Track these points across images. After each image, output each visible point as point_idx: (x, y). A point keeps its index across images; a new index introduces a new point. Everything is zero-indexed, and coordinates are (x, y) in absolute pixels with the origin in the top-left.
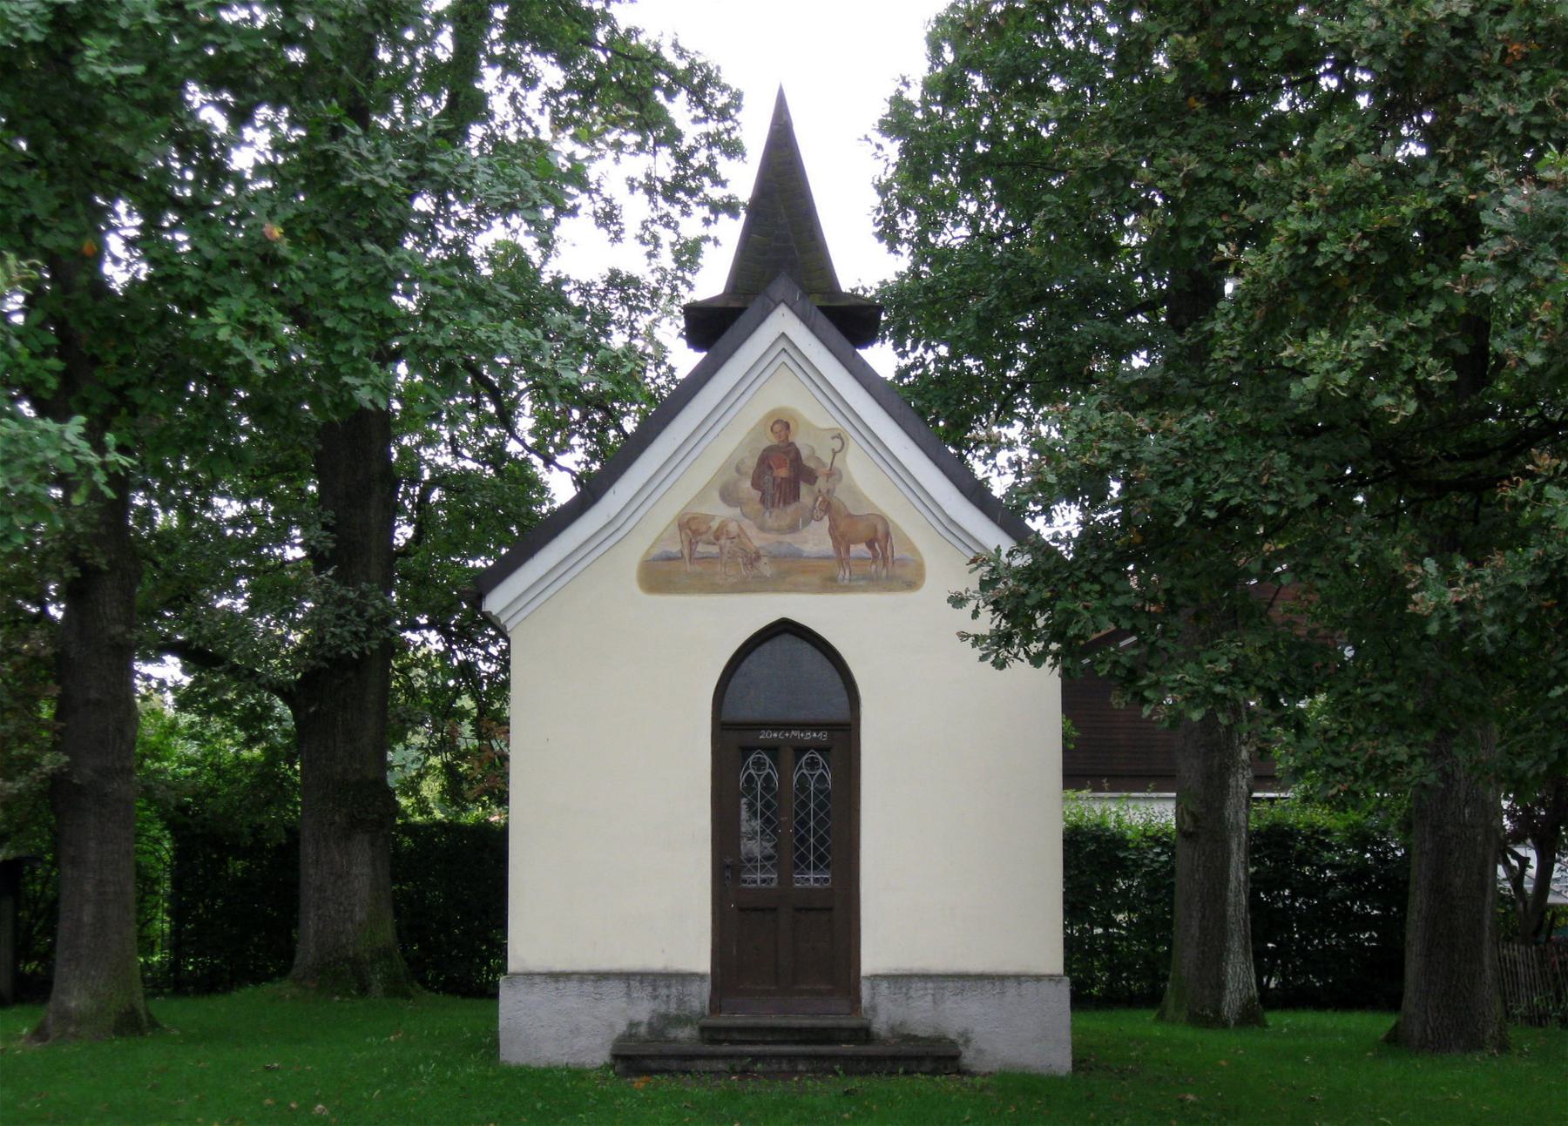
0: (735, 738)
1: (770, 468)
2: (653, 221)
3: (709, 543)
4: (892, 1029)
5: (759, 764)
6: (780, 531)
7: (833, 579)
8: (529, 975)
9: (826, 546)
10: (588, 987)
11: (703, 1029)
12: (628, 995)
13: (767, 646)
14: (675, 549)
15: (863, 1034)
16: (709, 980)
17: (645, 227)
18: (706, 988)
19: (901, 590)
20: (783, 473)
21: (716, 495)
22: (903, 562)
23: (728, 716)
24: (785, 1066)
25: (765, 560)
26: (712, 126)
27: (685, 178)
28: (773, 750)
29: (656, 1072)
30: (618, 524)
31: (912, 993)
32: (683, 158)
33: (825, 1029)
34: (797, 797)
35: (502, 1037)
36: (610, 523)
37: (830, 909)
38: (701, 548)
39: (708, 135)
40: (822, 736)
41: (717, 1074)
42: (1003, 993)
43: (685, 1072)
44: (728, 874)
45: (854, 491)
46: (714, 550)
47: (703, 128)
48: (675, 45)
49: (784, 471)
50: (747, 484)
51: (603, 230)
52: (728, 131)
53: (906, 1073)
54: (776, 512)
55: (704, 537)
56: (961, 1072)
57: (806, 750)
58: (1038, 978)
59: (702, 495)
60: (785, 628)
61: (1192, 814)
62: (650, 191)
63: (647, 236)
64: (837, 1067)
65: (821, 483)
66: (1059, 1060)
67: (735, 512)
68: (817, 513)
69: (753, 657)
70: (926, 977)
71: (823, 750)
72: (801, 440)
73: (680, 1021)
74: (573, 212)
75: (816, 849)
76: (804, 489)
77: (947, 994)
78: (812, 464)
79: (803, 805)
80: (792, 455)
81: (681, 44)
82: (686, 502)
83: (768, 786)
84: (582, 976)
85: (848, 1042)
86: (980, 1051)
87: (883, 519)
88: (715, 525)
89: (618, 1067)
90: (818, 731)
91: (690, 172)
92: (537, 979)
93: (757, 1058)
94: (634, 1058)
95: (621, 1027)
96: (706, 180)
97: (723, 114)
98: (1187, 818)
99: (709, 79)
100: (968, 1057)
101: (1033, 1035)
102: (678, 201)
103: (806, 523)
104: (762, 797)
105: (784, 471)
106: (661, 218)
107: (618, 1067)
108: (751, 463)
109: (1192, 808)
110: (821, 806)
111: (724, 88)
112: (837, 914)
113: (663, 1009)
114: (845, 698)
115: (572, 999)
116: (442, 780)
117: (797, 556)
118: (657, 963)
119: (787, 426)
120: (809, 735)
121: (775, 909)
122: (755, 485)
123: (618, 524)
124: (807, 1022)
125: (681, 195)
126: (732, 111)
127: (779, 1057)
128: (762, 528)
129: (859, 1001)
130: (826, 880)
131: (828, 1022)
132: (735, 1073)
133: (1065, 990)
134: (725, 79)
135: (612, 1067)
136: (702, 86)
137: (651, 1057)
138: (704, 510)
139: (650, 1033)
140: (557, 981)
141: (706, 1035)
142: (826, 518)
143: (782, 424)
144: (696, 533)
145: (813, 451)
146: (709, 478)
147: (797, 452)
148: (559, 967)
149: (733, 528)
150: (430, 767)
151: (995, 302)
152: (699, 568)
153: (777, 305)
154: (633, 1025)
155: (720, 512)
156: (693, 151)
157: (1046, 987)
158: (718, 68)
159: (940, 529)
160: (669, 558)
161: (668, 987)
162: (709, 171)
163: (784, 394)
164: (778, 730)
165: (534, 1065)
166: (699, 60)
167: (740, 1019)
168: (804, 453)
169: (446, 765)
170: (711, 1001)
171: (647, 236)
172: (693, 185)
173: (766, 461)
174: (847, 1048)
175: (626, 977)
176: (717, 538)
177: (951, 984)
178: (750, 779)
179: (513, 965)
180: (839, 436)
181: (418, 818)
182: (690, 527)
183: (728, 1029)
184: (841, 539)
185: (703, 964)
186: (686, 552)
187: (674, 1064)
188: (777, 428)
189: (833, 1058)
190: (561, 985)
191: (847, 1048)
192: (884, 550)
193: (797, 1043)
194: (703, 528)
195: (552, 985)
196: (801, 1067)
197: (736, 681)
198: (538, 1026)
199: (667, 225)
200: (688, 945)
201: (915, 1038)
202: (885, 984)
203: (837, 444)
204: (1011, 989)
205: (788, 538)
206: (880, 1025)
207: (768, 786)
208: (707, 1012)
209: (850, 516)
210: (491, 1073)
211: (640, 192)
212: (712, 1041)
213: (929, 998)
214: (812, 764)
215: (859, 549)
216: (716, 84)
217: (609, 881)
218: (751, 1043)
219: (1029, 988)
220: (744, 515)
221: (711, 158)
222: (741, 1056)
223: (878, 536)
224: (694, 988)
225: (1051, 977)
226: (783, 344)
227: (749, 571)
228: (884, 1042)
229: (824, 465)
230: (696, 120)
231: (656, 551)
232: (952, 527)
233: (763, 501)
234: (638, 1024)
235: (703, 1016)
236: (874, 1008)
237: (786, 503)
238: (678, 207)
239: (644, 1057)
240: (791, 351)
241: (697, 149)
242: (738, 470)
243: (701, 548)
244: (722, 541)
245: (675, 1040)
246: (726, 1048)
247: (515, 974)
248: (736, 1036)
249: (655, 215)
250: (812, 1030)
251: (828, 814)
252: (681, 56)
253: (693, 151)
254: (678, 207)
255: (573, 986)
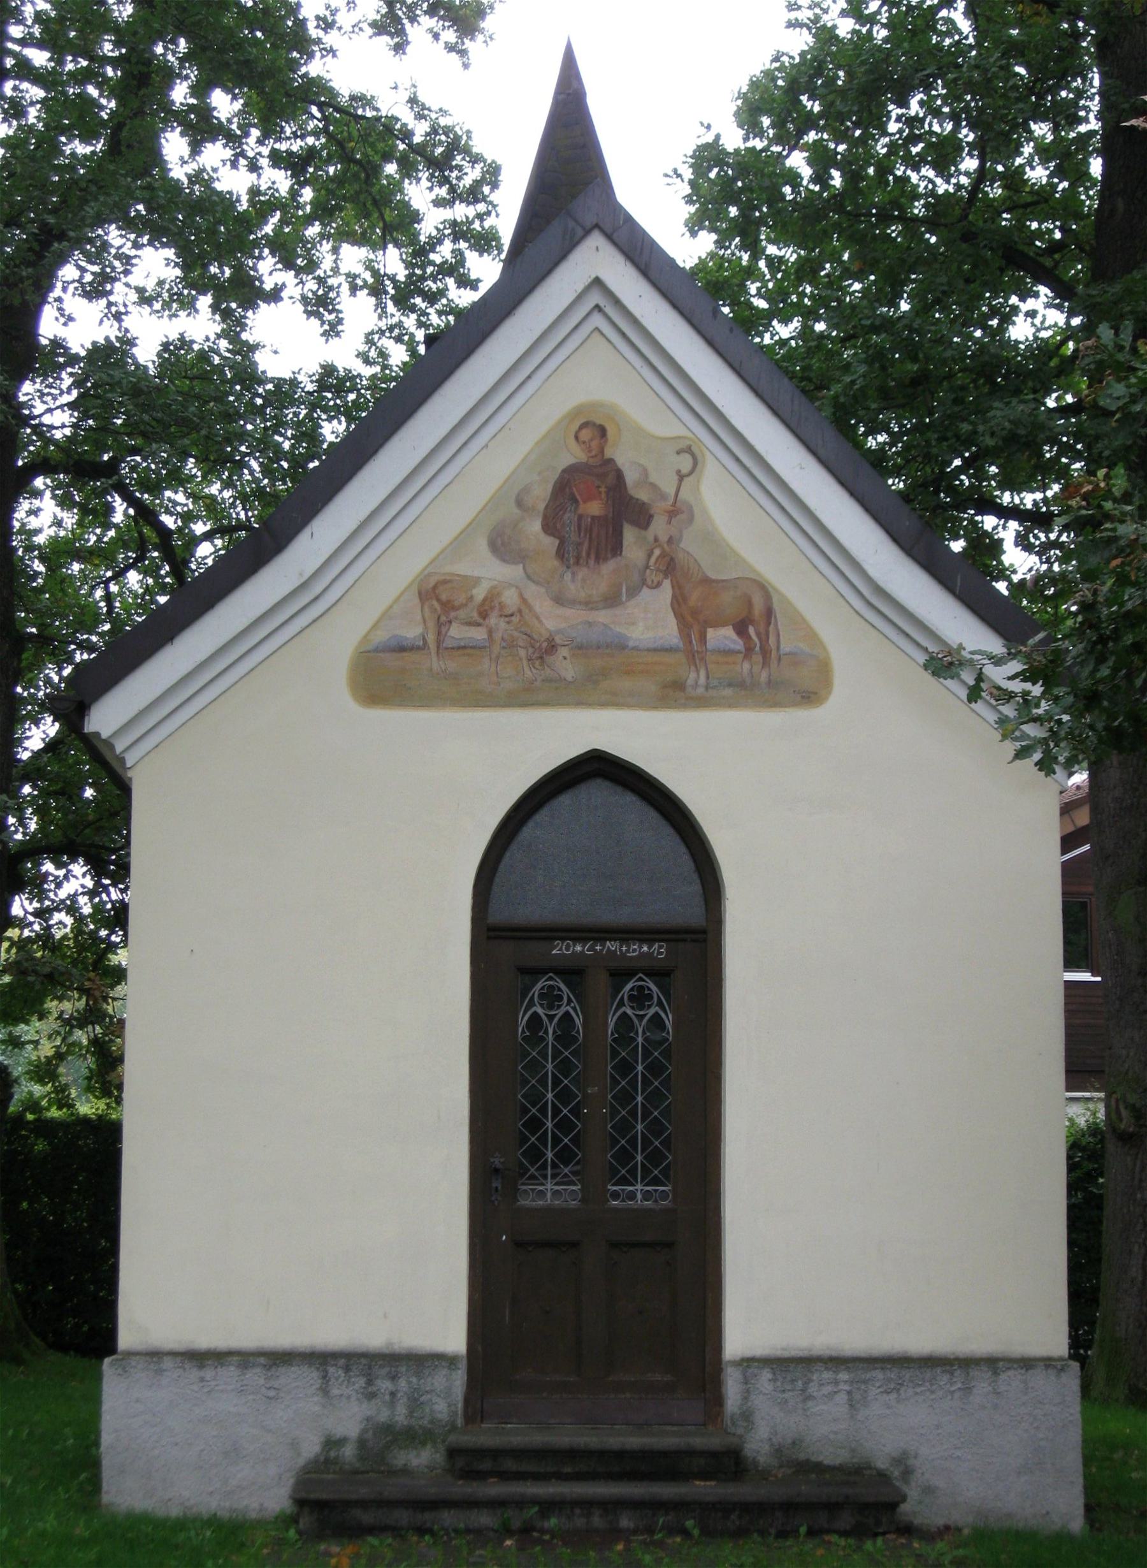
0: (511, 952)
1: (576, 501)
2: (382, 332)
3: (470, 624)
4: (778, 1451)
5: (551, 998)
6: (589, 604)
7: (678, 686)
8: (155, 1355)
9: (668, 631)
10: (255, 1377)
11: (453, 1453)
12: (325, 1391)
13: (565, 800)
14: (412, 632)
15: (729, 1463)
16: (463, 1365)
17: (369, 341)
18: (459, 1380)
19: (794, 704)
20: (594, 508)
21: (482, 544)
22: (796, 659)
23: (498, 915)
24: (597, 1521)
25: (564, 652)
26: (461, 211)
27: (423, 278)
28: (573, 973)
29: (371, 1530)
30: (318, 588)
31: (813, 1389)
32: (419, 253)
33: (665, 1454)
34: (615, 1053)
35: (105, 1463)
36: (304, 586)
37: (670, 1245)
38: (457, 632)
39: (454, 224)
40: (659, 950)
41: (477, 1535)
42: (967, 1390)
43: (421, 1531)
44: (496, 1183)
45: (711, 538)
46: (478, 634)
47: (446, 214)
48: (413, 101)
49: (596, 507)
50: (535, 526)
51: (314, 322)
52: (480, 217)
53: (811, 1533)
54: (582, 572)
55: (462, 614)
56: (907, 1530)
57: (629, 974)
58: (1026, 1363)
59: (459, 544)
60: (597, 767)
61: (1133, 1108)
62: (376, 291)
63: (373, 354)
64: (689, 1524)
65: (659, 527)
66: (1062, 1504)
67: (513, 572)
68: (652, 576)
69: (542, 816)
70: (836, 1362)
71: (660, 974)
72: (624, 456)
73: (411, 1437)
74: (275, 295)
75: (646, 1142)
76: (629, 534)
77: (873, 1391)
78: (643, 495)
79: (625, 1067)
80: (611, 479)
81: (421, 98)
82: (432, 555)
83: (566, 1033)
84: (245, 1359)
85: (705, 1476)
86: (929, 1490)
87: (763, 588)
88: (479, 593)
89: (305, 1522)
90: (650, 942)
91: (430, 269)
92: (168, 1363)
93: (548, 1506)
94: (329, 1504)
95: (311, 1448)
96: (450, 282)
97: (473, 195)
98: (1124, 1113)
99: (457, 146)
100: (913, 1508)
101: (1014, 1459)
102: (413, 309)
103: (633, 592)
104: (556, 1053)
105: (596, 507)
106: (391, 329)
107: (305, 1522)
108: (541, 493)
109: (1132, 1098)
110: (655, 1069)
111: (475, 159)
112: (683, 1252)
113: (384, 1416)
114: (697, 887)
115: (226, 1396)
116: (91, 1061)
117: (620, 646)
118: (372, 1335)
119: (602, 431)
120: (636, 950)
121: (574, 1245)
122: (549, 527)
123: (318, 588)
124: (634, 1441)
125: (418, 300)
126: (486, 189)
127: (587, 1505)
128: (559, 600)
129: (718, 1400)
130: (615, 1195)
131: (668, 1440)
132: (508, 1532)
133: (1072, 1380)
134: (477, 147)
135: (294, 1520)
136: (449, 155)
137: (363, 1504)
138: (463, 568)
139: (361, 1458)
140: (201, 1367)
141: (460, 1463)
142: (667, 584)
143: (594, 429)
144: (448, 606)
145: (645, 472)
146: (472, 515)
147: (619, 475)
148: (204, 1341)
149: (510, 598)
150: (74, 1044)
151: (860, 383)
152: (452, 665)
153: (587, 233)
154: (332, 1443)
155: (488, 571)
156: (434, 243)
157: (1040, 1380)
158: (468, 132)
159: (858, 604)
160: (401, 648)
161: (394, 1378)
162: (454, 269)
163: (598, 378)
164: (583, 940)
165: (161, 1512)
166: (443, 122)
167: (517, 1435)
168: (631, 477)
169: (95, 1042)
170: (467, 1401)
171: (373, 354)
172: (434, 287)
173: (566, 488)
174: (704, 1489)
175: (321, 1360)
176: (484, 615)
177: (879, 1374)
178: (535, 1022)
179: (126, 1339)
180: (689, 450)
181: (54, 1113)
182: (438, 596)
183: (496, 1454)
184: (692, 619)
185: (453, 1339)
186: (431, 638)
187: (403, 1517)
188: (585, 434)
189: (680, 1506)
190: (208, 1373)
191: (704, 1489)
192: (764, 637)
193: (611, 1477)
194: (461, 599)
195: (194, 1374)
196: (625, 1522)
197: (513, 856)
198: (160, 1444)
199: (399, 339)
200: (435, 1313)
201: (819, 1468)
202: (766, 1375)
203: (686, 463)
204: (982, 1384)
205: (602, 616)
206: (758, 1444)
207: (566, 1033)
208: (460, 1422)
209: (706, 581)
210: (80, 1530)
211: (363, 294)
212: (470, 1475)
213: (842, 1398)
214: (640, 998)
215: (722, 636)
216: (466, 151)
217: (296, 1190)
218: (537, 1477)
219: (1011, 1380)
220: (529, 577)
221: (459, 254)
222: (520, 1503)
223: (755, 616)
224: (439, 1380)
225: (1048, 1362)
226: (595, 298)
227: (537, 672)
228: (764, 1475)
229: (663, 497)
230: (438, 203)
231: (381, 636)
232: (879, 600)
233: (561, 554)
234: (341, 1442)
235: (453, 1428)
236: (747, 1416)
237: (600, 558)
238: (414, 316)
239: (348, 1504)
240: (610, 310)
241: (440, 242)
242: (519, 503)
243: (457, 632)
244: (493, 620)
245: (405, 1471)
246: (494, 1489)
247: (130, 1354)
248: (510, 1465)
249: (383, 324)
250: (645, 1454)
251: (666, 1083)
252: (420, 117)
253: (434, 243)
254: (414, 316)
255: (229, 1374)
